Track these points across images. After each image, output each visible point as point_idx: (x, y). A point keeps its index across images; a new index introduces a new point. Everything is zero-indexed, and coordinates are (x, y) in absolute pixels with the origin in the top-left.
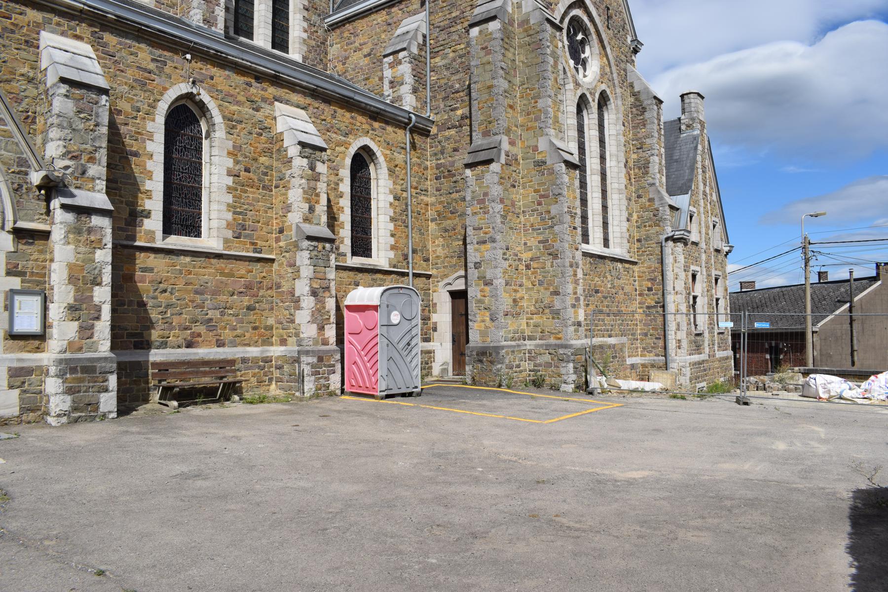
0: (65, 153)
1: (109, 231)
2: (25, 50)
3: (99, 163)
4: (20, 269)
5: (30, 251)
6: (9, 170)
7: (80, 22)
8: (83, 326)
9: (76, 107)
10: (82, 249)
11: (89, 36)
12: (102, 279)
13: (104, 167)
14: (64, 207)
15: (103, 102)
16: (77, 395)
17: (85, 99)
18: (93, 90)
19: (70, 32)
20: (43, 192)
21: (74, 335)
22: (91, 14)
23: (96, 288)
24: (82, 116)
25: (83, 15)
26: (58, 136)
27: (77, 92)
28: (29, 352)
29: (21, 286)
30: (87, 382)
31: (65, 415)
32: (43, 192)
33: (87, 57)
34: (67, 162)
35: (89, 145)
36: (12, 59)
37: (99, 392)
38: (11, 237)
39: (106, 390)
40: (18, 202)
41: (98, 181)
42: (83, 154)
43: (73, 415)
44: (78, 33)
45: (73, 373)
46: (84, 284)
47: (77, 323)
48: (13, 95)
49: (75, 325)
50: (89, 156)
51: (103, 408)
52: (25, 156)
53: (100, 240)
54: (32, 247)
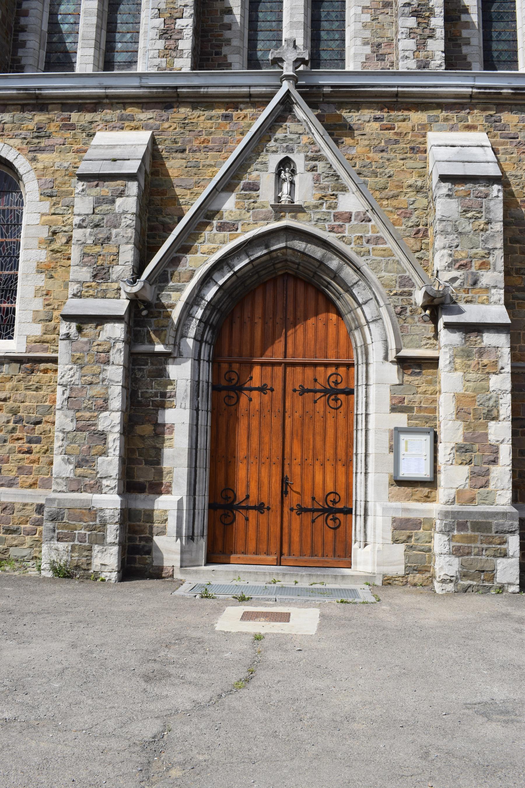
0: (451, 263)
1: (506, 351)
2: (411, 158)
3: (494, 268)
4: (406, 404)
5: (417, 382)
6: (391, 292)
7: (471, 110)
8: (476, 471)
9: (462, 207)
10: (472, 376)
11: (484, 123)
12: (498, 412)
13: (500, 272)
14: (448, 326)
15: (495, 193)
16: (466, 557)
17: (471, 195)
18: (481, 182)
19: (460, 125)
20: (428, 312)
21: (463, 482)
22: (483, 96)
23: (492, 424)
24: (469, 215)
25: (473, 101)
26: (442, 245)
27: (463, 188)
28: (418, 501)
29: (408, 423)
30: (480, 542)
31: (451, 581)
32: (428, 312)
33: (478, 146)
34: (454, 273)
35: (480, 249)
36: (398, 171)
37: (495, 556)
38: (395, 367)
39: (505, 555)
40: (402, 327)
41: (493, 291)
42: (474, 260)
43: (462, 583)
44: (470, 123)
45: (462, 530)
46: (475, 419)
47: (467, 467)
48: (401, 211)
49: (466, 470)
50: (481, 262)
51: (501, 578)
52: (407, 274)
53: (496, 363)
54: (419, 378)
